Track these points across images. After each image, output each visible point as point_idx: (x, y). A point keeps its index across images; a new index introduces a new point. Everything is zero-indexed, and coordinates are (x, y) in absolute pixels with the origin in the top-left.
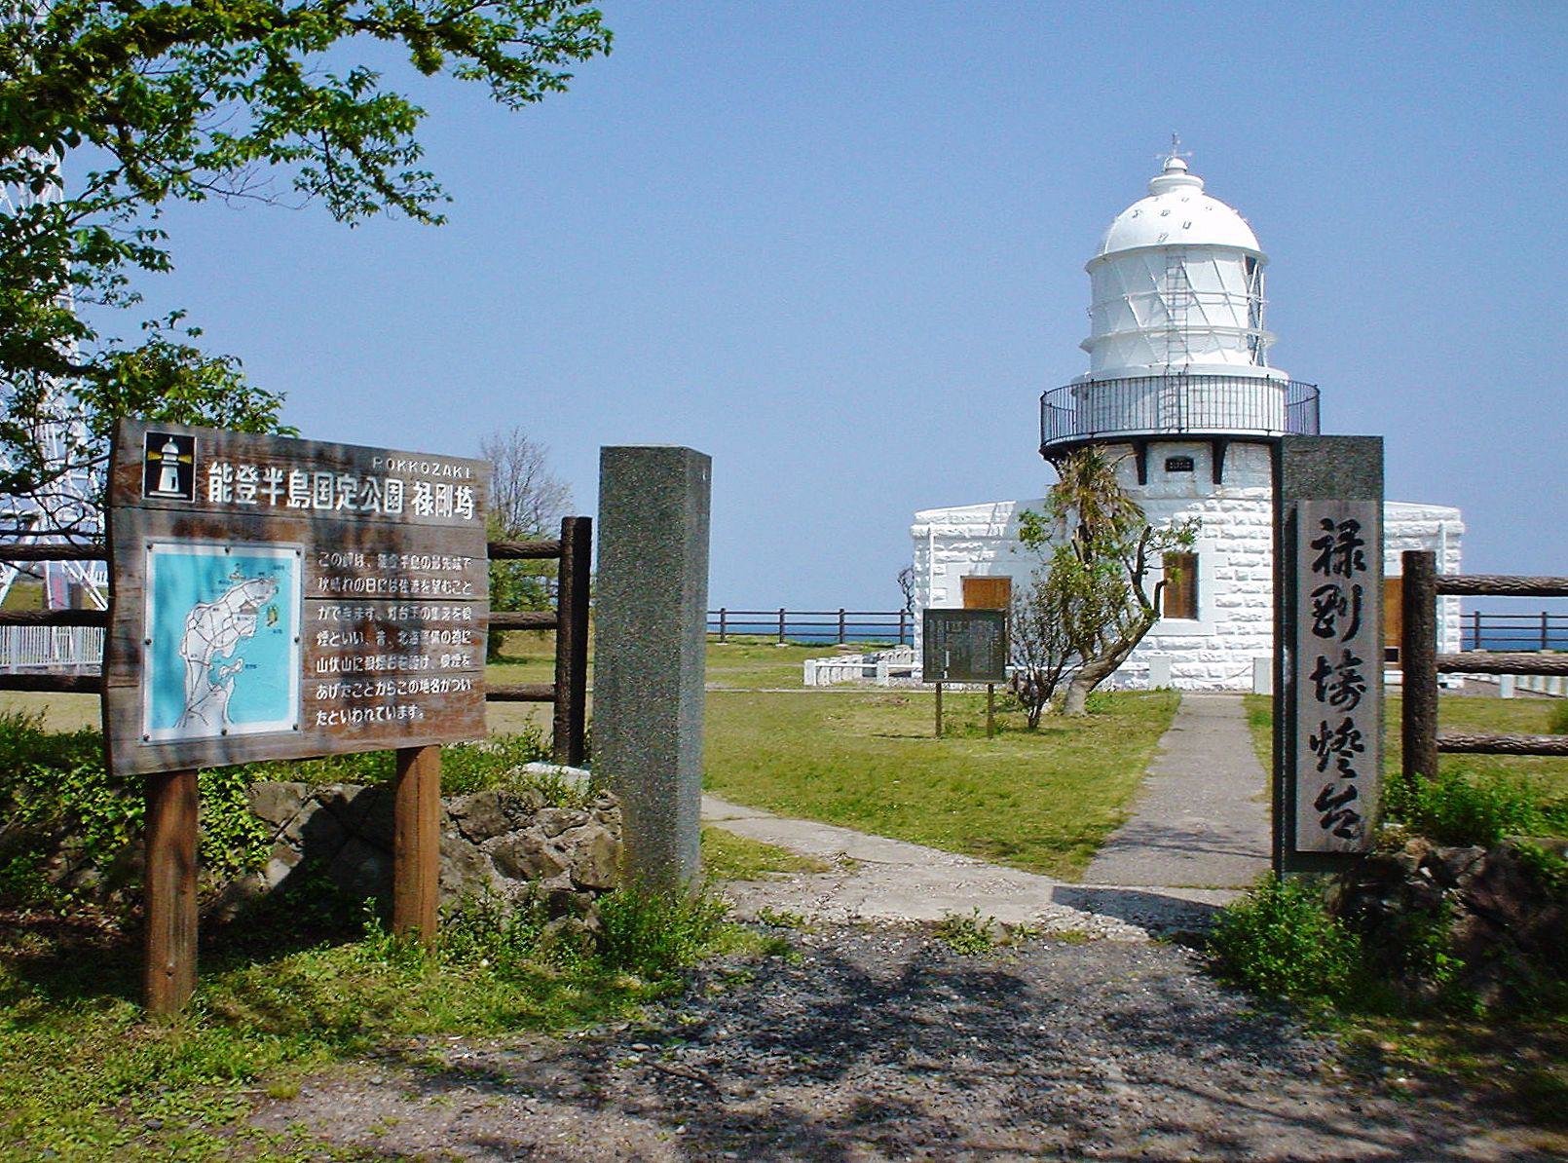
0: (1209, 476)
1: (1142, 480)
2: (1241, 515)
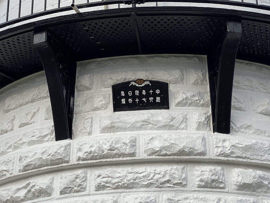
0: (201, 113)
1: (64, 127)
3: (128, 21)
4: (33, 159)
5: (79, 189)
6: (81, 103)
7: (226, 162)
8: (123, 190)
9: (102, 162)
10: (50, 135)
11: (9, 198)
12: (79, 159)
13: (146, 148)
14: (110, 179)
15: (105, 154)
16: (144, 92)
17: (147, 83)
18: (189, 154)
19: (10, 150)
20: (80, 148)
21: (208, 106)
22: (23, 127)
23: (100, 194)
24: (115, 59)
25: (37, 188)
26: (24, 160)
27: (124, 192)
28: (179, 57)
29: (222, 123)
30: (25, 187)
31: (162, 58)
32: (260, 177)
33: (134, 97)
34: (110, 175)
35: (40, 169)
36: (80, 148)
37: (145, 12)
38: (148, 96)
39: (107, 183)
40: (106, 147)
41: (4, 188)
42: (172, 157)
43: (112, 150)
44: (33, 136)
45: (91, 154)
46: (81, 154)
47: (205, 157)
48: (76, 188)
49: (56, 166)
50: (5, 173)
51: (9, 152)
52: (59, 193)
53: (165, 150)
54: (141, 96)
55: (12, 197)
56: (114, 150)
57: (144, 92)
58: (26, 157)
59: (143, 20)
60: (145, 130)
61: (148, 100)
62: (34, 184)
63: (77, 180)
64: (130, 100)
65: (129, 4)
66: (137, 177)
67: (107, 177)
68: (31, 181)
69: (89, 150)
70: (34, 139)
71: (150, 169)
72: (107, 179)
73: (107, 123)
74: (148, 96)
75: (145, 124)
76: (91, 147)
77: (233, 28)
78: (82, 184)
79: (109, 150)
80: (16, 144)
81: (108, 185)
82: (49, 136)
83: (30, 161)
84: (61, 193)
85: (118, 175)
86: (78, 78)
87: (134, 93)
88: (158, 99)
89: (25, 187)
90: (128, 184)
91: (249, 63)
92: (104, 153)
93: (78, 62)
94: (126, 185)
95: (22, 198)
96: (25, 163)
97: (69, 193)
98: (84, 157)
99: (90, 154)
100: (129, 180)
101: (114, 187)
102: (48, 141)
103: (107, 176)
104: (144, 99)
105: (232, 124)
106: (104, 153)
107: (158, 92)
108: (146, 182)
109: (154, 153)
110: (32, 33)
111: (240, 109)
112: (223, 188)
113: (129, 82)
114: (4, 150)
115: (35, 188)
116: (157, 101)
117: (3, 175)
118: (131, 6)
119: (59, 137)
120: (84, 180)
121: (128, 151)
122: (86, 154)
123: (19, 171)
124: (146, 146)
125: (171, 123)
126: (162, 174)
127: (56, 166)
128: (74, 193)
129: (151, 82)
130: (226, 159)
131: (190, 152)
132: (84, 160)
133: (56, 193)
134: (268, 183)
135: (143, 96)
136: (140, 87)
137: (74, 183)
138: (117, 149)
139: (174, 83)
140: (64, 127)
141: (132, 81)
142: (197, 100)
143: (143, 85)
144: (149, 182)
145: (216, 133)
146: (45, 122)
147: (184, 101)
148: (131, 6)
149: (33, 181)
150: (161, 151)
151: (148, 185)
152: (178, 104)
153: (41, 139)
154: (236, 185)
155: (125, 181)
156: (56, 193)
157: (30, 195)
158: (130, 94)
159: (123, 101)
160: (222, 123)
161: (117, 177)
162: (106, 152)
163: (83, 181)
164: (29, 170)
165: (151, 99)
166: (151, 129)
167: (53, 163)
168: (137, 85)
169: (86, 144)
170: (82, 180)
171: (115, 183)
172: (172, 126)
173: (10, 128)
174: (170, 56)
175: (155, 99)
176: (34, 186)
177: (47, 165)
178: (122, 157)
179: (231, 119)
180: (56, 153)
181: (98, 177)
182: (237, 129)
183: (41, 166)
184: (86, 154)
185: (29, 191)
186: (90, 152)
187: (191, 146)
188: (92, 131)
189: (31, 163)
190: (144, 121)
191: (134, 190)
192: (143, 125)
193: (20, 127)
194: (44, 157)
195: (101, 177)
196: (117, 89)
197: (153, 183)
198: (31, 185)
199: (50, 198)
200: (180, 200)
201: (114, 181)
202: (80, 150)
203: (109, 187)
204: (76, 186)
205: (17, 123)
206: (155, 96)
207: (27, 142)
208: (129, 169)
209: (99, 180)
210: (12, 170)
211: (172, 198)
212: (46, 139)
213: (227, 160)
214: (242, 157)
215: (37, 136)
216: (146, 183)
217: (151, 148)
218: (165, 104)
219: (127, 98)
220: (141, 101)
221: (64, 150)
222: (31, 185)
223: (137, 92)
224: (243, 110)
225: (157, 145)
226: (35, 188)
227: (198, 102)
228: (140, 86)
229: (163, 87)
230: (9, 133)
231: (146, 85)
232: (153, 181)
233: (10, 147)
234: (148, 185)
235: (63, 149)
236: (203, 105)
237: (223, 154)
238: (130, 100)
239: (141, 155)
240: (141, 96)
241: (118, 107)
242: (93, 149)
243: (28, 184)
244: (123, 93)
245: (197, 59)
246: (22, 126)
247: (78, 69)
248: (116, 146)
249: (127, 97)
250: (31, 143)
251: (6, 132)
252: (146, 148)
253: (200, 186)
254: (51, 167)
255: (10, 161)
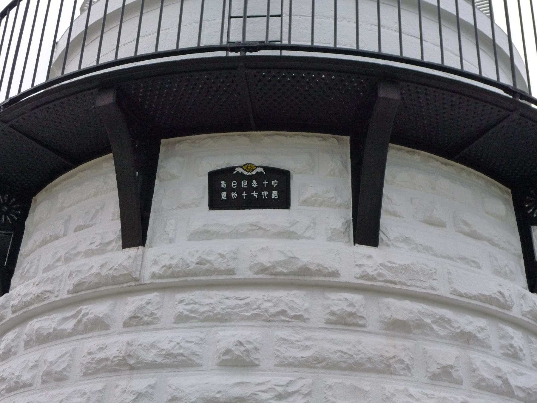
1: (135, 230)
2: (447, 354)
3: (235, 77)
4: (87, 275)
5: (150, 319)
6: (162, 198)
7: (370, 289)
8: (215, 323)
9: (186, 281)
10: (116, 242)
11: (51, 331)
12: (154, 276)
13: (252, 263)
14: (196, 306)
15: (191, 270)
16: (255, 184)
17: (260, 170)
18: (319, 272)
19: (60, 263)
20: (156, 260)
21: (348, 208)
22: (79, 230)
23: (180, 328)
24: (215, 137)
25: (90, 316)
26: (75, 276)
27: (217, 326)
28: (308, 136)
29: (366, 229)
30: (73, 317)
31: (283, 137)
32: (419, 312)
33: (239, 190)
34: (197, 301)
35: (98, 290)
36: (156, 260)
37: (214, 277)
38: (259, 189)
39: (192, 311)
40: (193, 260)
41: (48, 317)
42: (291, 277)
43: (201, 264)
44: (91, 244)
45: (171, 269)
46: (156, 269)
47: (336, 280)
48: (146, 318)
49: (125, 286)
50: (48, 295)
51: (57, 266)
52: (121, 325)
53: (281, 266)
54: (250, 188)
55: (55, 329)
56: (204, 264)
57: (255, 184)
58: (79, 271)
59: (255, 76)
60: (250, 237)
61: (260, 195)
62: (87, 311)
63: (149, 307)
64: (234, 195)
65: (237, 52)
66: (236, 305)
67: (192, 304)
68: (84, 307)
69: (168, 263)
70: (93, 247)
71: (254, 295)
72: (192, 306)
73: (197, 224)
74: (259, 189)
75: (257, 230)
76: (171, 258)
77: (388, 94)
78: (156, 312)
79: (197, 264)
80: (67, 255)
81: (192, 315)
82: (114, 244)
83: (83, 277)
84: (126, 324)
85: (208, 301)
86: (162, 161)
87: (239, 184)
88: (275, 194)
89: (73, 317)
90: (222, 315)
91: (411, 151)
92: (190, 268)
93: (162, 140)
94: (219, 316)
95: (69, 331)
96: (76, 280)
97: (136, 325)
98: (161, 273)
99: (170, 268)
100: (224, 309)
101: (201, 318)
102: (112, 250)
103: (192, 302)
104: (254, 194)
105: (381, 235)
106: (190, 268)
107: (275, 183)
108: (250, 312)
109: (264, 270)
110: (95, 91)
111: (394, 214)
112: (363, 326)
113: (233, 168)
114: (51, 264)
115: (87, 317)
116: (273, 197)
117: (45, 298)
118: (238, 54)
119: (126, 244)
120: (159, 306)
121: (224, 267)
122: (164, 269)
123: (68, 291)
124: (252, 260)
125: (292, 229)
126: (274, 301)
127: (125, 286)
128: (142, 325)
129: (265, 168)
130: (369, 283)
131: (317, 270)
132: (161, 277)
133: (118, 326)
134: (432, 321)
135: (255, 190)
136: (249, 175)
137: (143, 310)
138: (209, 262)
139: (301, 173)
140: (135, 230)
141: (238, 167)
142: (332, 198)
143: (254, 173)
144: (254, 312)
145: (357, 245)
146: (111, 225)
147: (313, 199)
148: (238, 54)
149: (85, 308)
150: (274, 267)
151: (255, 317)
152: (305, 202)
153: (103, 249)
154: (384, 322)
155: (218, 310)
156: (118, 326)
157: (81, 327)
158: (234, 186)
159: (224, 195)
160: (366, 229)
161: (207, 304)
162: (193, 266)
163: (158, 309)
164: (81, 291)
165: (265, 193)
166: (262, 236)
167: (114, 280)
168: (245, 173)
169: (165, 254)
170: (156, 307)
171: (203, 312)
172: (294, 233)
173: (62, 233)
174: (296, 135)
175: (270, 195)
176: (87, 314)
177: (106, 285)
178: (216, 275)
179: (381, 228)
180: (119, 266)
181: (179, 303)
182: (389, 242)
183: (97, 285)
184: (164, 269)
185: (80, 321)
186: (169, 265)
187: (319, 262)
188: (175, 236)
189: (85, 280)
190: (252, 225)
191: (233, 323)
192: (250, 230)
193: (76, 231)
194: (104, 272)
195: (184, 303)
196: (215, 177)
197: (259, 314)
198: (83, 312)
199: (109, 331)
200: (298, 341)
201: (202, 309)
202: (155, 263)
203: (194, 318)
204: (146, 315)
205: (72, 226)
206: (270, 190)
207: (84, 251)
208: (228, 293)
209: (181, 308)
210: (59, 290)
211: (287, 338)
212: (110, 248)
213: (372, 285)
214: (395, 283)
215: (97, 243)
216: (249, 314)
217: (259, 263)
218: (284, 202)
219: (230, 191)
220: (249, 196)
221: (133, 262)
222: (83, 312)
223: (244, 183)
224: (399, 216)
225: (265, 259)
226: (87, 317)
227: (333, 200)
228: (249, 174)
229: (284, 177)
230: (60, 240)
231: (257, 172)
232: (260, 311)
233: (59, 259)
234: (255, 317)
235: (131, 260)
236: (340, 206)
237: (365, 276)
238: (234, 195)
239: (244, 272)
240: (250, 188)
241: (215, 203)
242: (174, 262)
243: (80, 311)
244: (223, 184)
245: (335, 140)
246: (78, 229)
247: (162, 150)
248: (208, 258)
249: (229, 190)
250: (89, 253)
251: (57, 238)
252: (252, 263)
253: (329, 322)
254: (114, 287)
255: (57, 277)
